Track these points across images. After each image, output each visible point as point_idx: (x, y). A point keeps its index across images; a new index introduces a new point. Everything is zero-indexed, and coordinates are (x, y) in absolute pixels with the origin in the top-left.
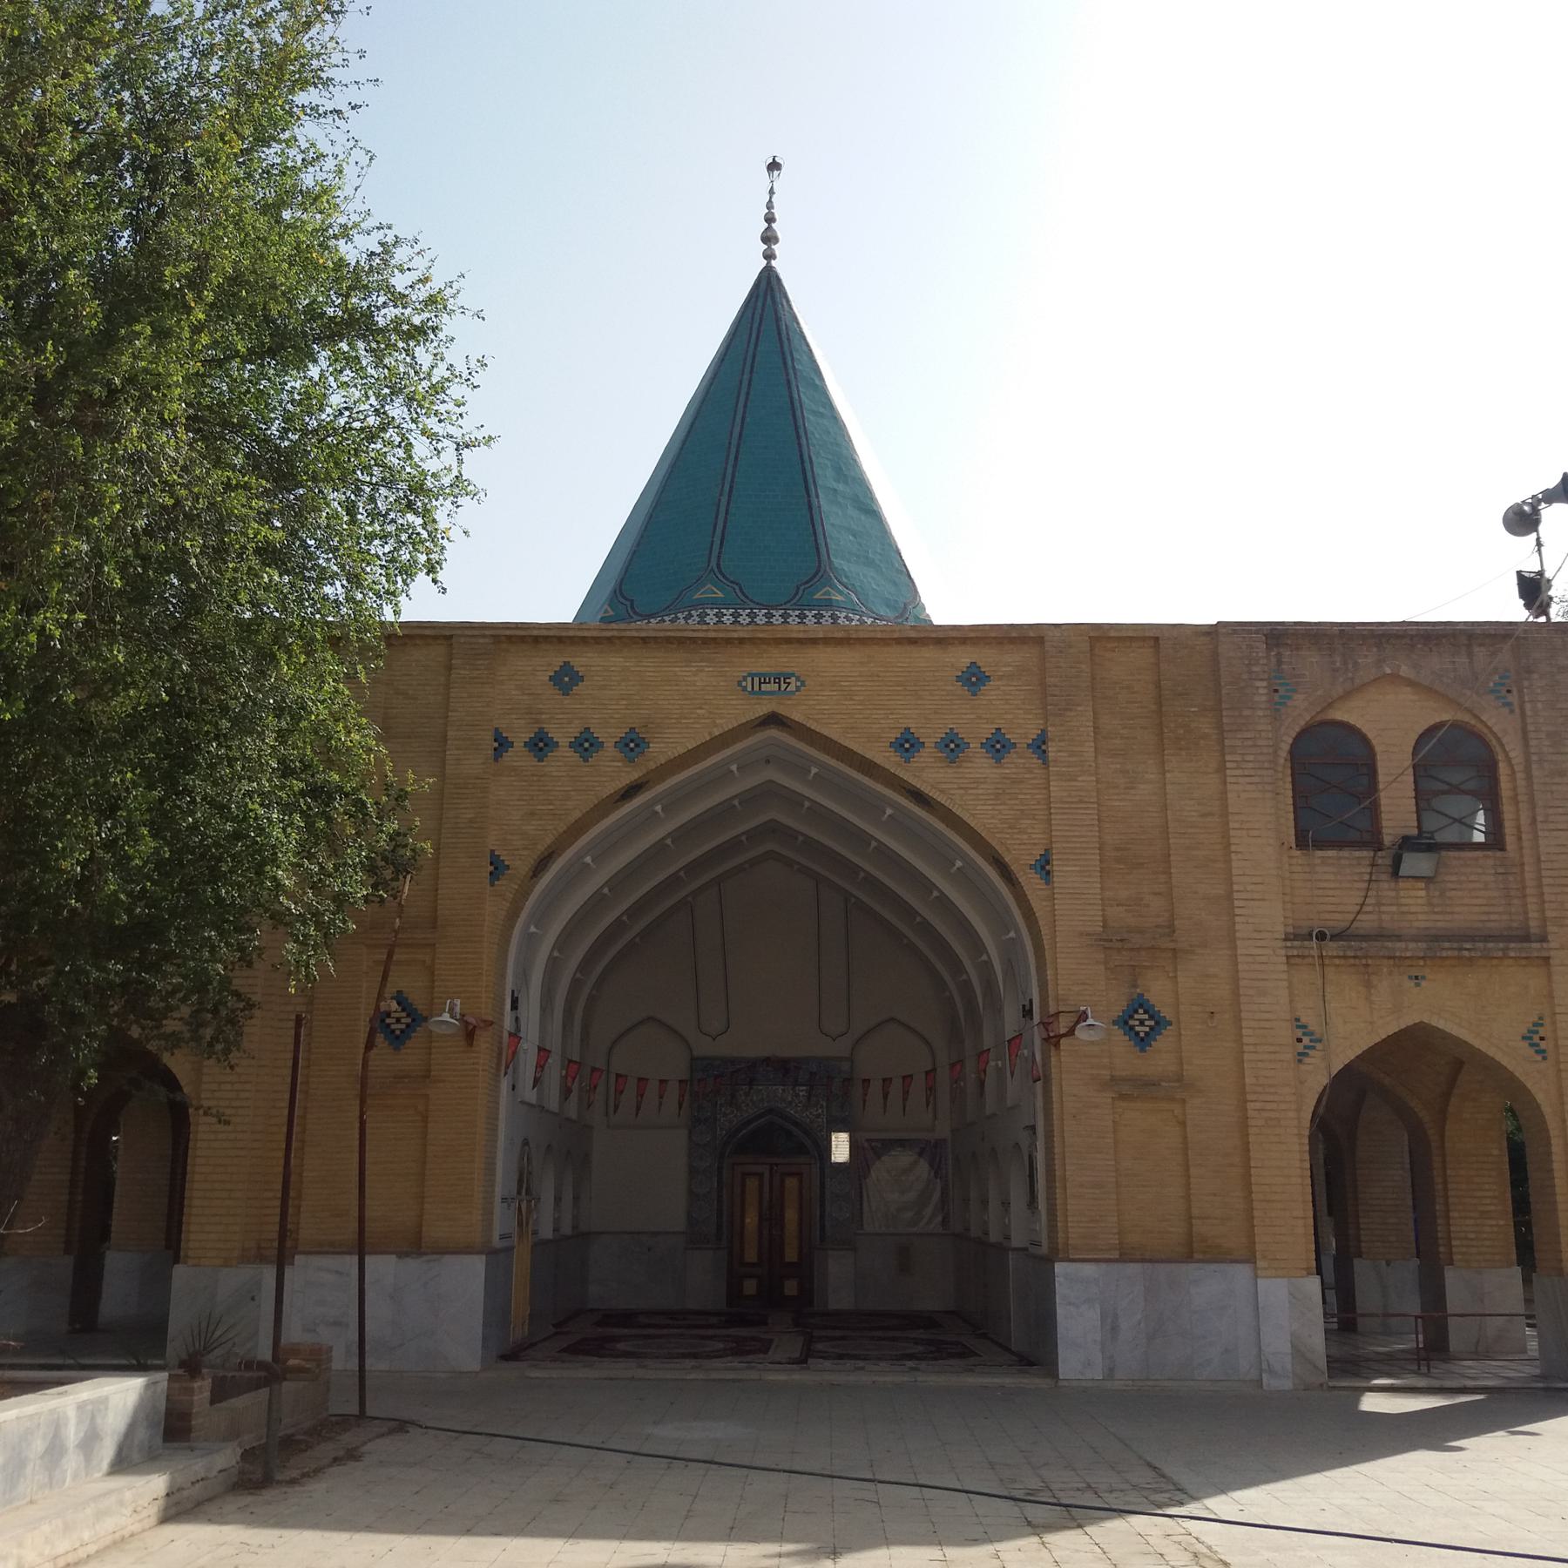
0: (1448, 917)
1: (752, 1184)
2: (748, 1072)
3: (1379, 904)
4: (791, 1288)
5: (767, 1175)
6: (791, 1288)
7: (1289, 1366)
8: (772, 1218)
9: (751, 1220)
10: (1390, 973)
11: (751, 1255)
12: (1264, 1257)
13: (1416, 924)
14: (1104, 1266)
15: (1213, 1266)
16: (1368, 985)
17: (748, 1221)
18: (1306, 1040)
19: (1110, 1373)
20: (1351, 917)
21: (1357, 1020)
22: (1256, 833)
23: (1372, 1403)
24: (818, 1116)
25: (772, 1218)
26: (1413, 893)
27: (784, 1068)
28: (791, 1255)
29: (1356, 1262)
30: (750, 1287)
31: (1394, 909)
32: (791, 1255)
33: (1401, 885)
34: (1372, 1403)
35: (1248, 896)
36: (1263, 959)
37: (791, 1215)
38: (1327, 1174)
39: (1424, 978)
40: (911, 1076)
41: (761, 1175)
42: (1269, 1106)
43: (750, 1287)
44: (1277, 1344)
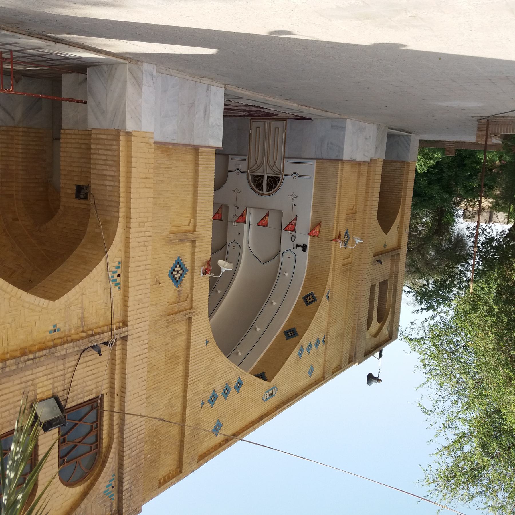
0: (23, 379)
3: (64, 375)
7: (144, 78)
10: (70, 330)
12: (151, 145)
13: (44, 368)
14: (207, 145)
15: (168, 141)
16: (82, 319)
18: (121, 278)
19: (209, 86)
20: (80, 361)
21: (88, 297)
22: (135, 396)
23: (211, 51)
26: (45, 389)
29: (220, 145)
31: (56, 374)
33: (50, 393)
34: (211, 51)
35: (142, 357)
36: (138, 321)
39: (50, 332)
42: (141, 234)
44: (148, 91)
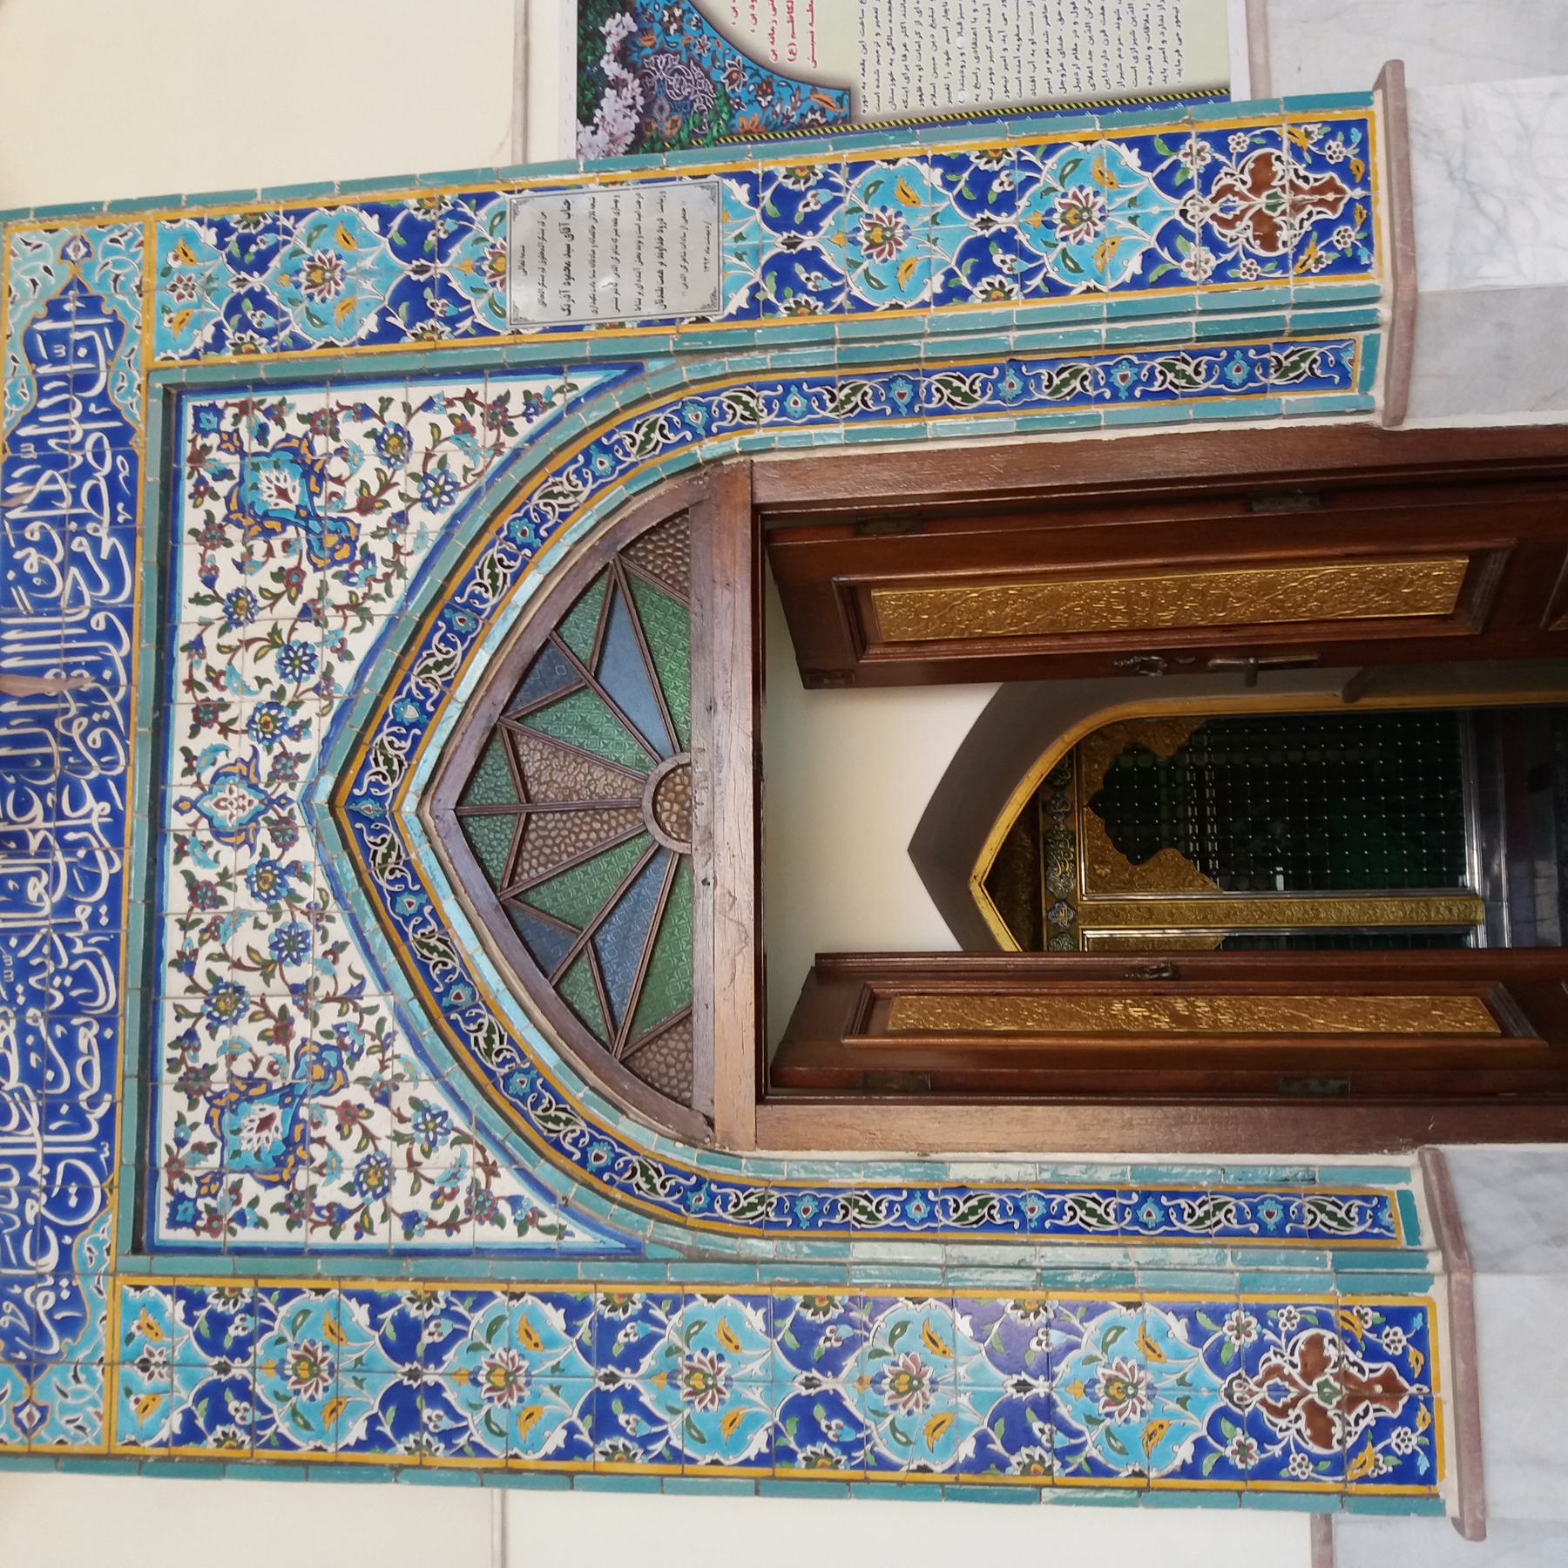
24: (392, 444)
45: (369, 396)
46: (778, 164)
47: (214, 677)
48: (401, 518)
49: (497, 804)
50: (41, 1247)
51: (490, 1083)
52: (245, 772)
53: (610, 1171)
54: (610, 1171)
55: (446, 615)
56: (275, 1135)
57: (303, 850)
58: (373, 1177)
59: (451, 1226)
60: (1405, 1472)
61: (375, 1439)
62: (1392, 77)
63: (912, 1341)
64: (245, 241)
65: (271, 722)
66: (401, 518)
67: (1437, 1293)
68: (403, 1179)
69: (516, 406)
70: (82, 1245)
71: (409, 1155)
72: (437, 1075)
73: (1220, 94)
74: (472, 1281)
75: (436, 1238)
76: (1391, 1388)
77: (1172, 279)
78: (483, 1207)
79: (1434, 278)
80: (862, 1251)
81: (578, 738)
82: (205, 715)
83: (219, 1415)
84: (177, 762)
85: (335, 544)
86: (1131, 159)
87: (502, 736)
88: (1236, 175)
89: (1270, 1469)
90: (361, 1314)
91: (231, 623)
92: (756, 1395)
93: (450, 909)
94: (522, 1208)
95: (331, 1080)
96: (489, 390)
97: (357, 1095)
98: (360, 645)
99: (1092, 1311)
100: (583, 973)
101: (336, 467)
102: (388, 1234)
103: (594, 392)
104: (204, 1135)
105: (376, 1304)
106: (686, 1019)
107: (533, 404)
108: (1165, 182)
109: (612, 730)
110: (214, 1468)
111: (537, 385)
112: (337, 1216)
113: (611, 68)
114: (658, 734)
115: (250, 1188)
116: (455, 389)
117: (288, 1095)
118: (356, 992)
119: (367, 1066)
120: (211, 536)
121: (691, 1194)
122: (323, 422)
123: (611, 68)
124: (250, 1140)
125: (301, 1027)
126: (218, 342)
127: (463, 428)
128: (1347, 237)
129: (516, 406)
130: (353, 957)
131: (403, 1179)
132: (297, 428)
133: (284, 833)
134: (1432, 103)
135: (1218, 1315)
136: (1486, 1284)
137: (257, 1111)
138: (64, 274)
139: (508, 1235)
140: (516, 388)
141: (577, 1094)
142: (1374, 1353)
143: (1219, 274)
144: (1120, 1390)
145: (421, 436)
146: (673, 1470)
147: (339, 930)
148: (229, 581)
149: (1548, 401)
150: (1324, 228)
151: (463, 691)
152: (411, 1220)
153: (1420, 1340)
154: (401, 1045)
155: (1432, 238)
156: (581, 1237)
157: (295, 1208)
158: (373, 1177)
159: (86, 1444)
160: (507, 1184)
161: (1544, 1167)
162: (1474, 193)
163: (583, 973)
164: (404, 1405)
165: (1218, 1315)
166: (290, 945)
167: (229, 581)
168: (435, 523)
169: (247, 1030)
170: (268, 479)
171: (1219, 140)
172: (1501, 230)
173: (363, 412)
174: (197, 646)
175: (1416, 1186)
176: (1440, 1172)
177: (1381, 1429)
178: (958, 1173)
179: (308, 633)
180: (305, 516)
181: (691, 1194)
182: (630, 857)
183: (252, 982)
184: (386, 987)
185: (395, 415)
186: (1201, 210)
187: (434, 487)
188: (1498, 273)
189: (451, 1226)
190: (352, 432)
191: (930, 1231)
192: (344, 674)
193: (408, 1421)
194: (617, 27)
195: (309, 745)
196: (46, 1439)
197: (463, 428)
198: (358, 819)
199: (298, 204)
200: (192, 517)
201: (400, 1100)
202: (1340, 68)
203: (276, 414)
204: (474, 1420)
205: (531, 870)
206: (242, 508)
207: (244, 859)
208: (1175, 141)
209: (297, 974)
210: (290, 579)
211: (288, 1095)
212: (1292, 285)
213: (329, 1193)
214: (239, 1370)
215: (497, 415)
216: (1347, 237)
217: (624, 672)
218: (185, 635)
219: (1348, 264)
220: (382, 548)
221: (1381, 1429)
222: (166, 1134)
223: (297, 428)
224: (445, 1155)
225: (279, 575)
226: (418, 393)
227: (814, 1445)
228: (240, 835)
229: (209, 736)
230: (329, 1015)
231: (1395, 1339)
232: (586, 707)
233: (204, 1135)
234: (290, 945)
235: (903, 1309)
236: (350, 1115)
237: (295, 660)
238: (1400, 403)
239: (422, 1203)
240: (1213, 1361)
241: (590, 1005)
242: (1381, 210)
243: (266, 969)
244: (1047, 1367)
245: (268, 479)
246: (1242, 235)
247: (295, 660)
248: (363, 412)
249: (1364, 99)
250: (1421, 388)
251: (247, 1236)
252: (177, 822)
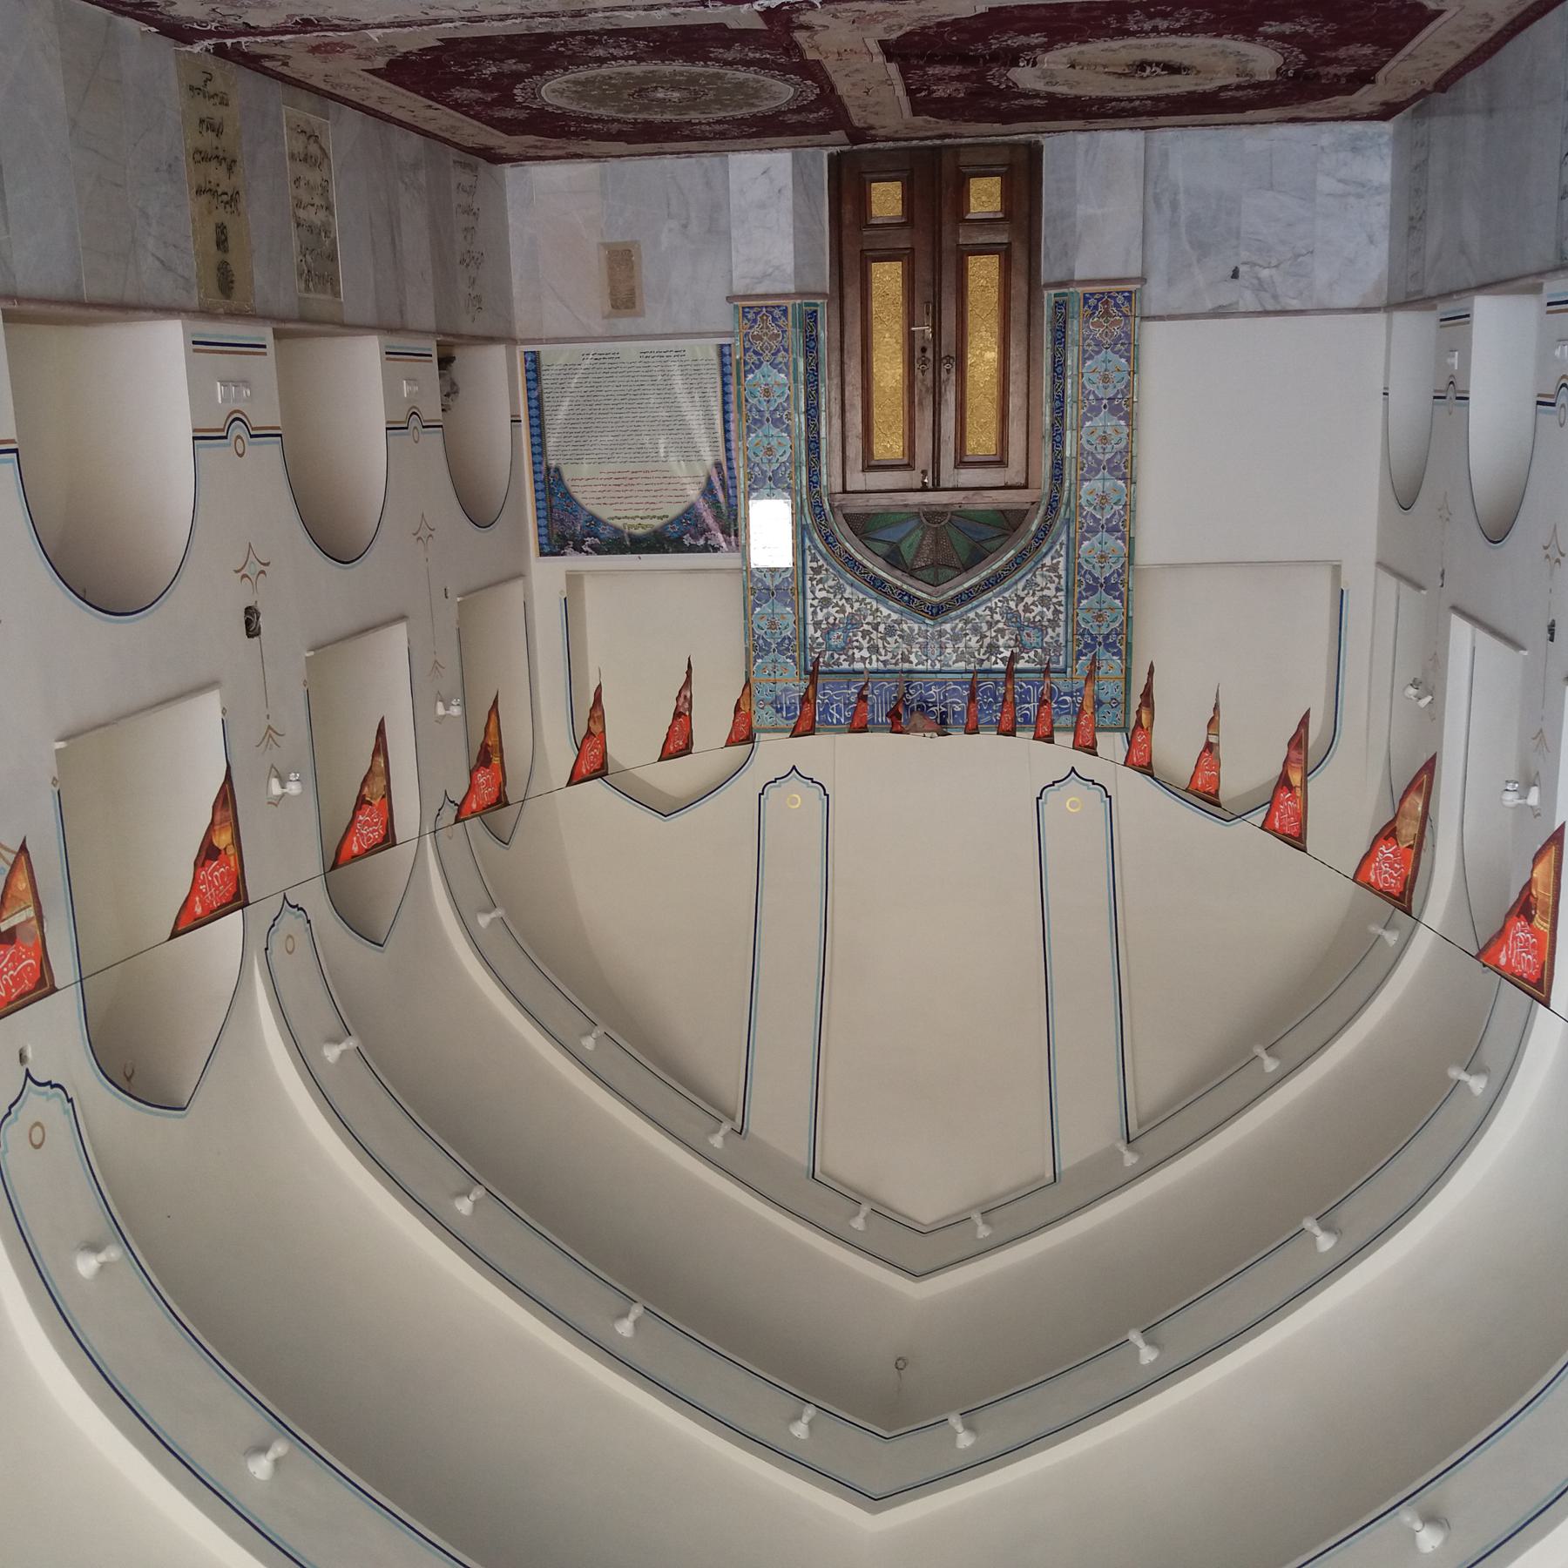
1: (981, 441)
2: (998, 703)
4: (886, 200)
5: (947, 460)
6: (886, 200)
8: (936, 360)
9: (983, 356)
11: (983, 273)
17: (992, 355)
24: (825, 602)
25: (936, 360)
27: (909, 709)
28: (887, 278)
30: (985, 197)
32: (887, 278)
37: (889, 370)
38: (598, 550)
40: (665, 756)
41: (1001, 462)
43: (985, 197)
45: (810, 610)
46: (742, 483)
47: (894, 657)
48: (847, 600)
49: (938, 569)
50: (1065, 702)
51: (1019, 566)
52: (924, 647)
53: (1045, 530)
54: (1045, 530)
55: (877, 585)
56: (1033, 632)
57: (947, 627)
58: (1044, 601)
59: (1059, 577)
60: (1128, 299)
61: (1120, 597)
62: (730, 299)
63: (1093, 439)
64: (761, 649)
65: (908, 639)
66: (847, 600)
67: (1080, 290)
68: (1046, 592)
69: (814, 565)
70: (1064, 689)
71: (1038, 591)
72: (1016, 583)
73: (722, 351)
74: (1074, 566)
75: (1063, 582)
76: (1107, 302)
77: (786, 364)
78: (1054, 568)
79: (791, 288)
80: (1068, 453)
81: (913, 551)
82: (905, 659)
83: (1113, 645)
84: (920, 667)
85: (853, 622)
86: (750, 376)
87: (911, 572)
88: (758, 346)
89: (1128, 336)
90: (1084, 602)
91: (878, 652)
92: (1107, 484)
93: (966, 585)
94: (1055, 558)
95: (1016, 615)
96: (809, 571)
97: (1021, 607)
98: (885, 612)
99: (1084, 387)
100: (987, 545)
101: (831, 620)
102: (1062, 596)
103: (812, 540)
104: (1032, 654)
105: (1081, 598)
106: (1002, 512)
107: (814, 559)
108: (758, 367)
109: (910, 540)
110: (1129, 645)
111: (809, 558)
112: (1056, 612)
113: (701, 542)
114: (913, 524)
115: (1047, 639)
116: (809, 584)
117: (1021, 628)
118: (990, 609)
119: (1012, 605)
120: (852, 659)
121: (1053, 507)
122: (817, 624)
123: (701, 542)
124: (1034, 640)
125: (1001, 625)
126: (791, 657)
127: (820, 581)
128: (777, 312)
129: (814, 565)
130: (979, 611)
131: (1046, 592)
132: (819, 634)
133: (941, 634)
134: (739, 287)
135: (1085, 351)
136: (1077, 276)
137: (1025, 638)
138: (769, 708)
139: (1062, 560)
140: (809, 564)
141: (1023, 543)
142: (1096, 307)
143: (786, 351)
144: (1105, 379)
145: (824, 594)
146: (1130, 508)
147: (972, 615)
148: (865, 653)
149: (823, 249)
150: (774, 319)
151: (899, 584)
152: (1058, 590)
153: (1092, 294)
154: (1006, 595)
155: (778, 288)
156: (1063, 538)
157: (1054, 623)
158: (1044, 601)
159: (1122, 685)
160: (1047, 561)
161: (1047, 255)
162: (765, 276)
163: (987, 545)
164: (1110, 588)
165: (1085, 351)
166: (976, 630)
167: (865, 653)
168: (849, 589)
169: (1001, 642)
170: (833, 642)
171: (746, 350)
172: (777, 268)
173: (814, 613)
174: (885, 662)
175: (1053, 292)
176: (1049, 286)
177: (1117, 305)
178: (1048, 427)
179: (882, 628)
180: (845, 631)
181: (1053, 507)
182: (953, 532)
183: (987, 641)
184: (990, 600)
185: (815, 602)
186: (767, 355)
187: (839, 589)
188: (790, 269)
189: (1059, 577)
190: (820, 616)
191: (1062, 435)
192: (895, 616)
193: (1114, 587)
194: (687, 540)
195: (916, 627)
196: (1121, 698)
197: (820, 581)
198: (937, 612)
199: (749, 632)
200: (845, 666)
201: (1022, 594)
202: (721, 317)
203: (814, 639)
204: (1115, 567)
205: (955, 562)
206: (843, 650)
207: (950, 645)
208: (745, 363)
209: (985, 627)
210: (865, 634)
211: (1021, 628)
212: (790, 329)
213: (1049, 615)
214: (1100, 639)
215: (817, 571)
216: (777, 312)
217: (892, 535)
218: (881, 666)
219: (785, 312)
220: (856, 605)
221: (1117, 305)
222: (1031, 666)
223: (819, 634)
224: (1039, 580)
225: (864, 637)
226: (809, 595)
227: (1124, 467)
228: (942, 647)
229: (912, 658)
230: (997, 617)
231: (1092, 302)
232: (904, 547)
233: (1032, 654)
234: (976, 630)
235: (1083, 441)
236: (1027, 609)
237: (890, 631)
238: (822, 295)
239: (1052, 586)
240: (1098, 353)
241: (996, 543)
242: (770, 303)
243: (983, 637)
244: (1098, 399)
245: (833, 642)
246: (774, 344)
247: (890, 631)
248: (814, 613)
249: (736, 307)
250: (819, 289)
251: (1062, 640)
252: (938, 666)
